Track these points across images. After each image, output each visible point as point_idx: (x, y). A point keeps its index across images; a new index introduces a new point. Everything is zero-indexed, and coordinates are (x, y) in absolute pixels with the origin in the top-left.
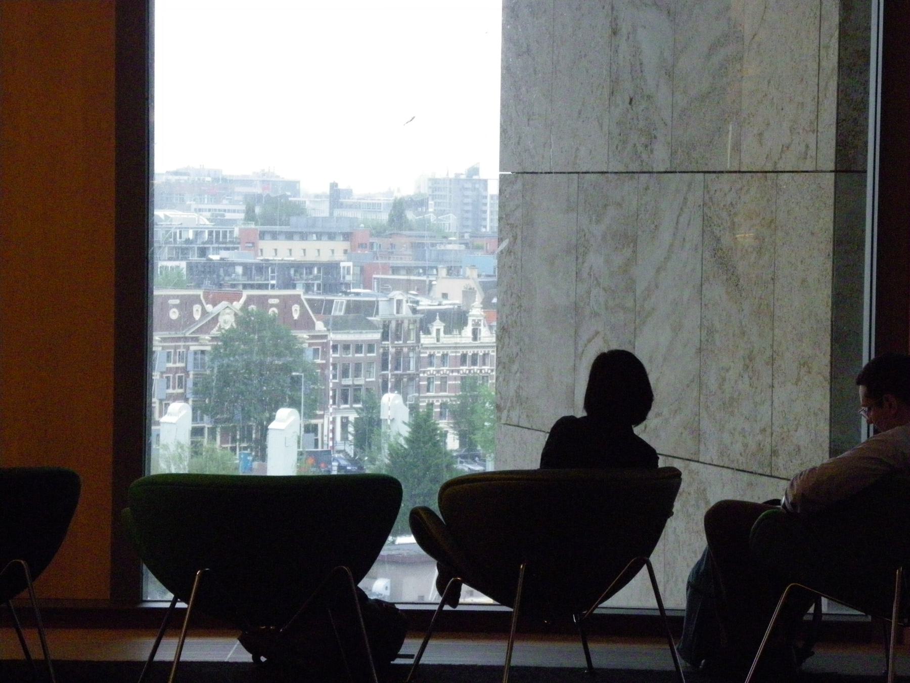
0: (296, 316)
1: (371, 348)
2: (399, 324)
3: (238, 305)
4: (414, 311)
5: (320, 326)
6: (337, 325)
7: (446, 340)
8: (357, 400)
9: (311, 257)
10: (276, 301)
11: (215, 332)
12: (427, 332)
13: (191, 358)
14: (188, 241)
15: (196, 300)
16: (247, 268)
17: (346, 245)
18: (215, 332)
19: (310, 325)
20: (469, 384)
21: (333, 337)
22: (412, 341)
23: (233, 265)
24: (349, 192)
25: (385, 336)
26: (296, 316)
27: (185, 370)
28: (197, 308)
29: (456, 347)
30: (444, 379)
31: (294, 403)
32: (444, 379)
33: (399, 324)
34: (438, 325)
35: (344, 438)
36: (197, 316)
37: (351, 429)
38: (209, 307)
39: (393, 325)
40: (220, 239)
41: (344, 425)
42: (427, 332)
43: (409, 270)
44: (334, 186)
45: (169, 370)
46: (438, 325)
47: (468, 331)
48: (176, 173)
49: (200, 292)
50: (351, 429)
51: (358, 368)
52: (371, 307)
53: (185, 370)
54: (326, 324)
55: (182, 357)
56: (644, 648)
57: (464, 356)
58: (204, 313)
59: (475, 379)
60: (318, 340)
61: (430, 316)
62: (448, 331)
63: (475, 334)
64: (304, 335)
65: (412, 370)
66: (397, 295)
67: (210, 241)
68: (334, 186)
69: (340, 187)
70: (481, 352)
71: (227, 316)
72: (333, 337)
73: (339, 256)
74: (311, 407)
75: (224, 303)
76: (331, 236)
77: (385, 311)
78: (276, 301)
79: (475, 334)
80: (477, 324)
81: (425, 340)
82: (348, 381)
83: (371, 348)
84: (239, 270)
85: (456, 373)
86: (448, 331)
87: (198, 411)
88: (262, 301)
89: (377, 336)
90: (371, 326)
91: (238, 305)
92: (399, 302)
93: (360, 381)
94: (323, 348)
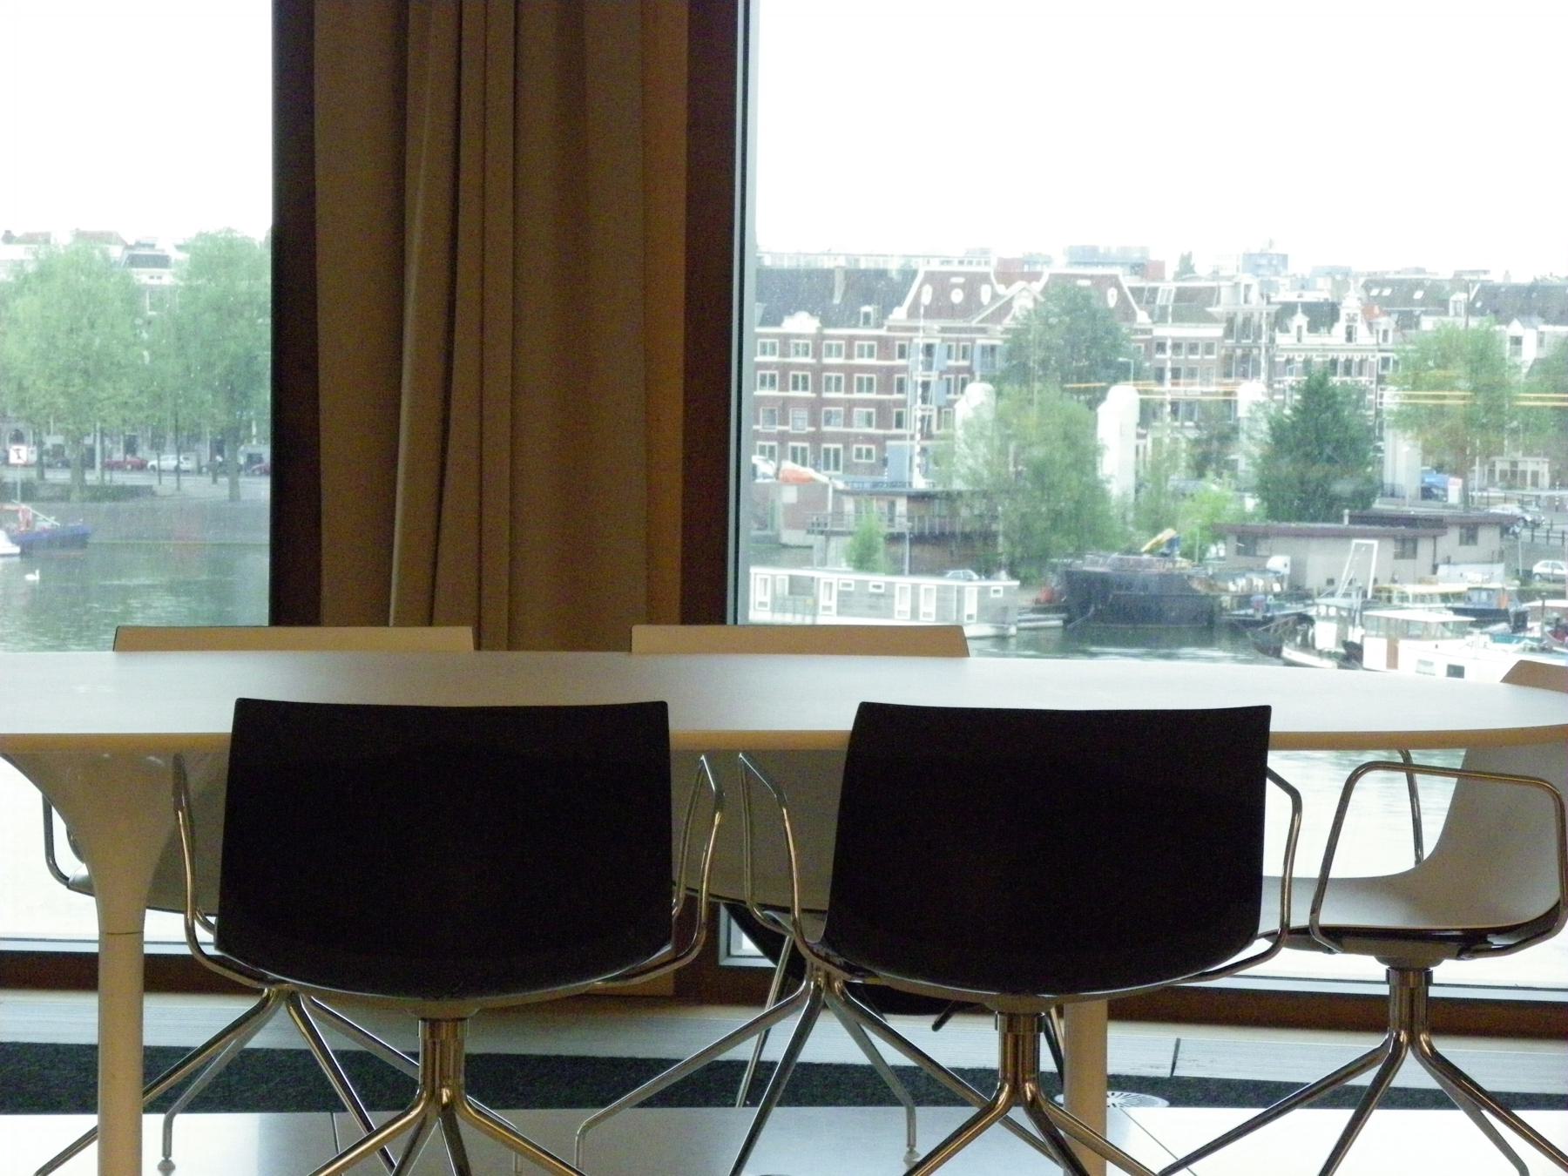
1: (1209, 349)
7: (1310, 340)
11: (1008, 322)
13: (977, 354)
25: (1229, 332)
29: (1325, 349)
34: (1300, 320)
38: (1001, 289)
39: (1239, 320)
45: (949, 370)
47: (1340, 328)
54: (1151, 315)
58: (995, 296)
61: (1288, 309)
62: (1313, 327)
75: (1020, 284)
80: (1352, 319)
81: (1282, 340)
83: (1209, 349)
86: (1313, 327)
90: (1210, 319)
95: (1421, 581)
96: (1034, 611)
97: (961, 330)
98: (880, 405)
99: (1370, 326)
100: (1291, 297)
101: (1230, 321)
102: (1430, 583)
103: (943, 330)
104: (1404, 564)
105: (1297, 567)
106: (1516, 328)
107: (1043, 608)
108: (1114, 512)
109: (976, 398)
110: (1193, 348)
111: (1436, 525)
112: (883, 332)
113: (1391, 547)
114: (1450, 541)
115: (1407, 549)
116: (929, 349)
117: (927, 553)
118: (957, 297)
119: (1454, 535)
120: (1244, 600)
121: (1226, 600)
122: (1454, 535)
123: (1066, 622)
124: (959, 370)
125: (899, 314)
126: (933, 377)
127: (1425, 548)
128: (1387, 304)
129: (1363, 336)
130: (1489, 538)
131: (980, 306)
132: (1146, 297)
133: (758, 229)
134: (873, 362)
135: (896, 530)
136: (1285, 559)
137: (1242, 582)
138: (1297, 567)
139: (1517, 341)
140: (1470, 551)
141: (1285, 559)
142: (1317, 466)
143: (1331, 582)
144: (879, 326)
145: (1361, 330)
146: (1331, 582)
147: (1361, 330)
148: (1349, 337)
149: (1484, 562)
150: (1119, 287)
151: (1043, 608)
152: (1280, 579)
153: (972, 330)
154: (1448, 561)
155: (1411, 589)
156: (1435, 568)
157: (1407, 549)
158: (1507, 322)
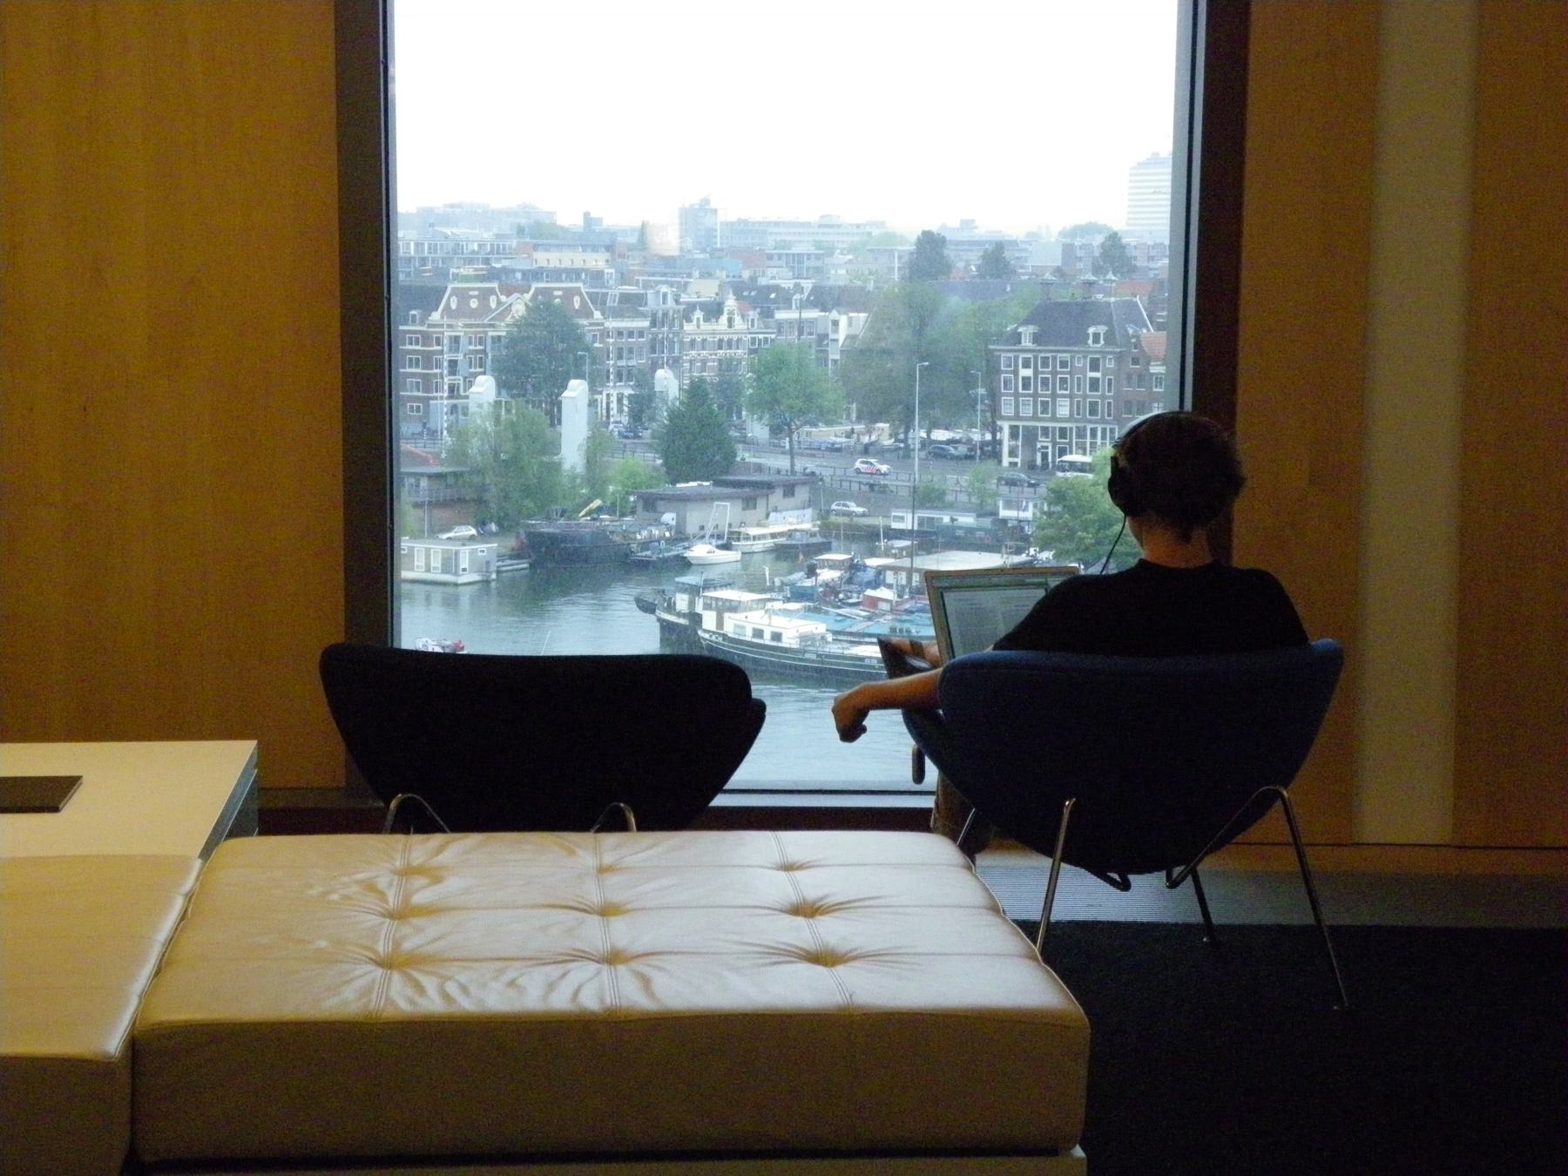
0: (577, 306)
1: (641, 334)
2: (665, 314)
3: (528, 296)
4: (677, 302)
5: (597, 315)
6: (618, 314)
7: (705, 327)
8: (629, 379)
9: (578, 264)
10: (560, 293)
11: (509, 320)
12: (689, 320)
13: (489, 342)
14: (473, 252)
15: (492, 291)
16: (524, 273)
17: (607, 255)
18: (509, 320)
19: (589, 315)
20: (727, 366)
21: (612, 324)
22: (676, 328)
23: (514, 271)
24: (600, 220)
25: (653, 324)
26: (577, 306)
27: (484, 351)
28: (493, 299)
29: (713, 333)
30: (704, 362)
31: (579, 376)
32: (704, 362)
33: (665, 314)
34: (698, 314)
35: (620, 411)
36: (493, 305)
37: (626, 402)
38: (503, 298)
39: (660, 314)
40: (498, 251)
41: (620, 401)
42: (689, 320)
43: (664, 275)
44: (587, 215)
45: (472, 352)
46: (698, 314)
47: (724, 319)
48: (452, 206)
49: (495, 285)
50: (626, 402)
51: (631, 351)
52: (639, 299)
53: (484, 351)
54: (603, 313)
55: (481, 341)
56: (354, 991)
57: (721, 341)
58: (499, 303)
59: (731, 360)
60: (600, 325)
61: (691, 307)
62: (706, 320)
63: (730, 321)
64: (584, 322)
65: (676, 354)
66: (664, 289)
67: (491, 252)
68: (587, 215)
69: (593, 215)
70: (735, 338)
71: (519, 306)
72: (612, 324)
73: (601, 265)
74: (596, 382)
75: (516, 295)
76: (595, 249)
77: (652, 303)
78: (560, 293)
79: (730, 321)
80: (731, 313)
81: (688, 327)
82: (622, 363)
83: (641, 334)
84: (519, 275)
85: (713, 356)
86: (706, 320)
87: (501, 385)
88: (547, 292)
89: (646, 324)
90: (643, 315)
91: (528, 296)
92: (665, 295)
93: (633, 363)
94: (606, 334)
95: (759, 525)
96: (511, 557)
97: (478, 326)
98: (424, 376)
99: (743, 316)
100: (694, 299)
101: (654, 315)
102: (764, 526)
103: (466, 326)
104: (749, 513)
105: (681, 523)
106: (834, 315)
107: (517, 555)
108: (565, 481)
109: (484, 388)
110: (631, 334)
111: (769, 486)
112: (424, 328)
113: (739, 504)
114: (777, 497)
115: (749, 503)
116: (456, 340)
117: (441, 514)
118: (474, 304)
119: (779, 492)
120: (645, 545)
121: (634, 546)
122: (779, 492)
123: (532, 566)
124: (477, 352)
125: (436, 316)
126: (460, 357)
127: (761, 503)
128: (754, 304)
129: (739, 324)
130: (802, 494)
131: (490, 310)
132: (599, 300)
133: (76, 797)
134: (418, 348)
135: (419, 500)
136: (674, 515)
137: (645, 533)
138: (681, 523)
139: (836, 323)
140: (791, 501)
141: (674, 515)
142: (697, 445)
143: (702, 528)
144: (422, 323)
145: (737, 319)
146: (702, 528)
147: (737, 319)
148: (730, 326)
149: (798, 509)
150: (581, 294)
151: (517, 555)
152: (669, 529)
153: (484, 326)
154: (776, 510)
155: (753, 531)
156: (768, 515)
157: (749, 503)
158: (830, 311)
